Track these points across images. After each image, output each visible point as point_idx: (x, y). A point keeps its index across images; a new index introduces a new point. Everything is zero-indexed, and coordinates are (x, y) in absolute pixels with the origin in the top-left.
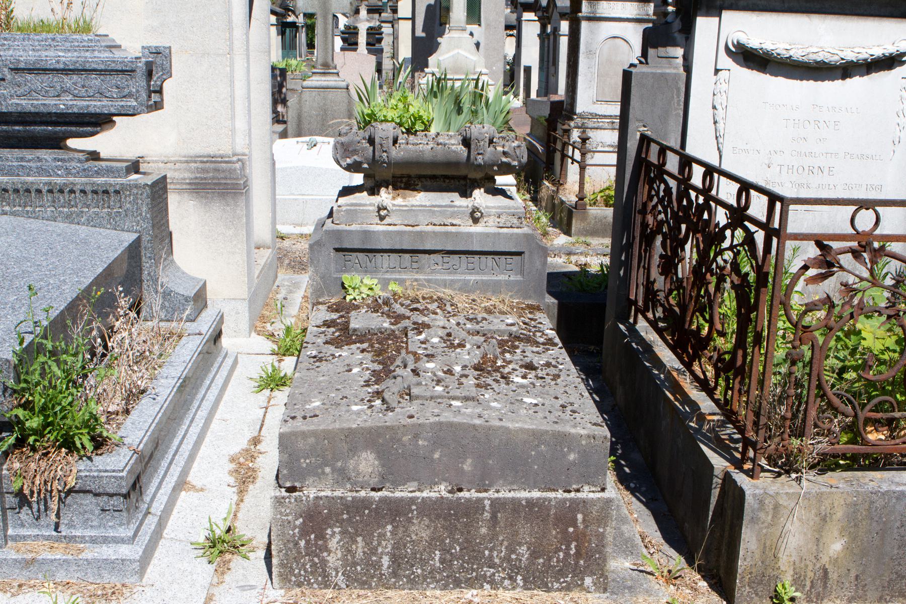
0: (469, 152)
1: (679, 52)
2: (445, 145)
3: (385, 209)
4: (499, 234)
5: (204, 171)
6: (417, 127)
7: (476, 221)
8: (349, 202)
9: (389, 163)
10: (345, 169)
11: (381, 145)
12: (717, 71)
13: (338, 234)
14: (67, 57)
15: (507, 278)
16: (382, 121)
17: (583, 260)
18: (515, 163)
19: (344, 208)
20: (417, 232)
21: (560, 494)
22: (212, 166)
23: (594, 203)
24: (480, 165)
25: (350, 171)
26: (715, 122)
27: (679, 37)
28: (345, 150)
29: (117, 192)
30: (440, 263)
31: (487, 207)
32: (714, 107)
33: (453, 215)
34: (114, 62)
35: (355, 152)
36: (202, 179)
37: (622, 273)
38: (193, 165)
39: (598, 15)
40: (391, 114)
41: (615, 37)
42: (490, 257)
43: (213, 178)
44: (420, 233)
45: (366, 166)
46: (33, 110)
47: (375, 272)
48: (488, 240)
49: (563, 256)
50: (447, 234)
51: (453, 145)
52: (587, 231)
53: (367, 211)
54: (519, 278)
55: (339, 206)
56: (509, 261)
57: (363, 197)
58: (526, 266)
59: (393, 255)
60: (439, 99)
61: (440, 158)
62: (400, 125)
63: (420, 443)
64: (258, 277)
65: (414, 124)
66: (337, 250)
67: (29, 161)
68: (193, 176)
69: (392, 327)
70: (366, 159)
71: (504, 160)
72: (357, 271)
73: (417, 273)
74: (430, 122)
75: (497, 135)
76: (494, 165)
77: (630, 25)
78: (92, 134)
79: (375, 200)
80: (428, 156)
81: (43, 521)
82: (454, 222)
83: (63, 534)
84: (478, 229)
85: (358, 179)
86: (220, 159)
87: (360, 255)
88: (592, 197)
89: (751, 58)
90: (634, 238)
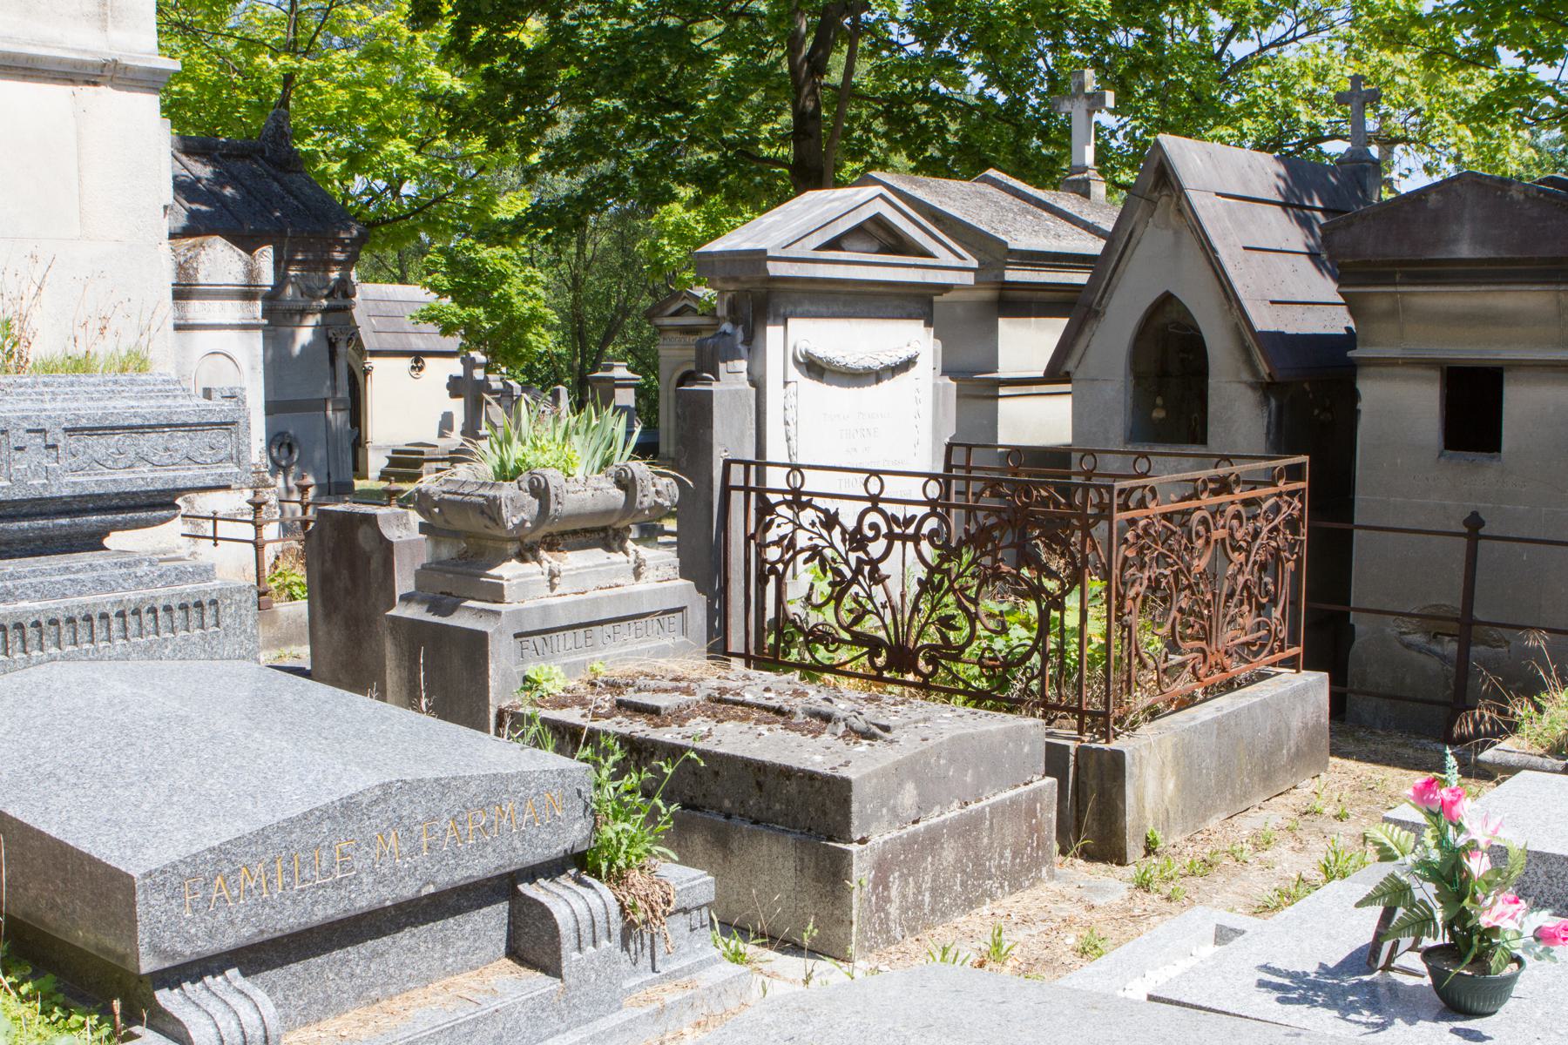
1: (742, 365)
12: (786, 383)
14: (148, 409)
18: (667, 503)
19: (515, 582)
21: (1022, 789)
26: (788, 439)
27: (743, 350)
29: (214, 602)
32: (787, 423)
34: (26, 418)
46: (98, 490)
66: (516, 636)
67: (78, 571)
78: (148, 524)
80: (589, 506)
81: (640, 966)
83: (663, 972)
84: (641, 586)
89: (815, 368)
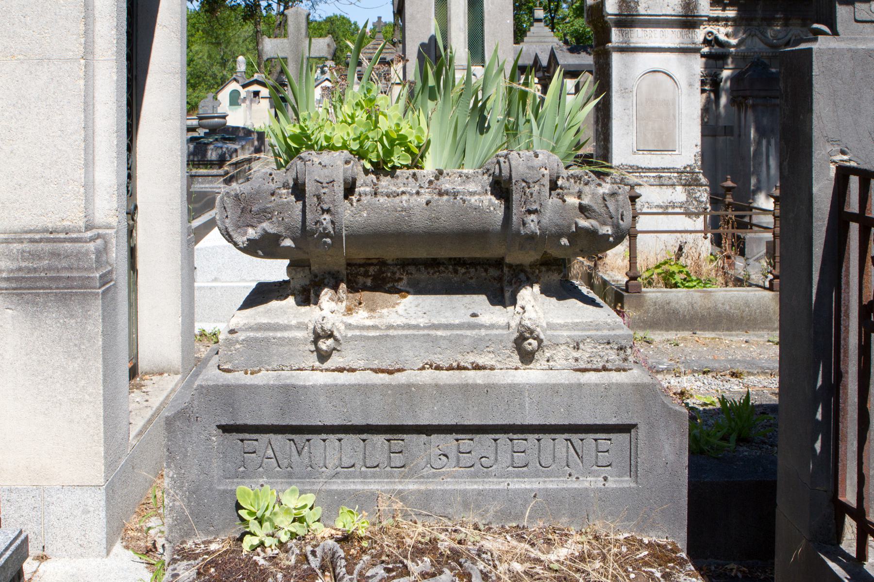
2: (455, 195)
3: (331, 335)
4: (580, 386)
5: (35, 256)
6: (396, 160)
7: (527, 357)
8: (252, 322)
10: (245, 250)
11: (319, 197)
16: (322, 148)
19: (241, 336)
20: (400, 386)
22: (48, 247)
24: (532, 237)
25: (256, 255)
28: (243, 210)
30: (452, 455)
31: (550, 326)
33: (477, 346)
35: (265, 214)
36: (29, 270)
37: (818, 446)
38: (16, 247)
39: (632, 45)
40: (340, 134)
41: (654, 71)
43: (50, 268)
44: (406, 388)
45: (288, 243)
47: (310, 476)
48: (557, 399)
50: (466, 389)
52: (644, 322)
53: (291, 342)
54: (627, 482)
55: (232, 332)
56: (604, 445)
57: (285, 310)
58: (642, 457)
59: (347, 438)
60: (440, 101)
61: (447, 221)
62: (361, 155)
64: (140, 433)
65: (389, 153)
66: (226, 429)
68: (13, 265)
70: (288, 228)
71: (583, 223)
74: (424, 148)
75: (565, 173)
76: (560, 236)
77: (673, 56)
79: (311, 315)
80: (420, 220)
82: (481, 361)
84: (532, 375)
85: (276, 270)
86: (62, 236)
87: (278, 439)
88: (647, 274)
90: (839, 375)
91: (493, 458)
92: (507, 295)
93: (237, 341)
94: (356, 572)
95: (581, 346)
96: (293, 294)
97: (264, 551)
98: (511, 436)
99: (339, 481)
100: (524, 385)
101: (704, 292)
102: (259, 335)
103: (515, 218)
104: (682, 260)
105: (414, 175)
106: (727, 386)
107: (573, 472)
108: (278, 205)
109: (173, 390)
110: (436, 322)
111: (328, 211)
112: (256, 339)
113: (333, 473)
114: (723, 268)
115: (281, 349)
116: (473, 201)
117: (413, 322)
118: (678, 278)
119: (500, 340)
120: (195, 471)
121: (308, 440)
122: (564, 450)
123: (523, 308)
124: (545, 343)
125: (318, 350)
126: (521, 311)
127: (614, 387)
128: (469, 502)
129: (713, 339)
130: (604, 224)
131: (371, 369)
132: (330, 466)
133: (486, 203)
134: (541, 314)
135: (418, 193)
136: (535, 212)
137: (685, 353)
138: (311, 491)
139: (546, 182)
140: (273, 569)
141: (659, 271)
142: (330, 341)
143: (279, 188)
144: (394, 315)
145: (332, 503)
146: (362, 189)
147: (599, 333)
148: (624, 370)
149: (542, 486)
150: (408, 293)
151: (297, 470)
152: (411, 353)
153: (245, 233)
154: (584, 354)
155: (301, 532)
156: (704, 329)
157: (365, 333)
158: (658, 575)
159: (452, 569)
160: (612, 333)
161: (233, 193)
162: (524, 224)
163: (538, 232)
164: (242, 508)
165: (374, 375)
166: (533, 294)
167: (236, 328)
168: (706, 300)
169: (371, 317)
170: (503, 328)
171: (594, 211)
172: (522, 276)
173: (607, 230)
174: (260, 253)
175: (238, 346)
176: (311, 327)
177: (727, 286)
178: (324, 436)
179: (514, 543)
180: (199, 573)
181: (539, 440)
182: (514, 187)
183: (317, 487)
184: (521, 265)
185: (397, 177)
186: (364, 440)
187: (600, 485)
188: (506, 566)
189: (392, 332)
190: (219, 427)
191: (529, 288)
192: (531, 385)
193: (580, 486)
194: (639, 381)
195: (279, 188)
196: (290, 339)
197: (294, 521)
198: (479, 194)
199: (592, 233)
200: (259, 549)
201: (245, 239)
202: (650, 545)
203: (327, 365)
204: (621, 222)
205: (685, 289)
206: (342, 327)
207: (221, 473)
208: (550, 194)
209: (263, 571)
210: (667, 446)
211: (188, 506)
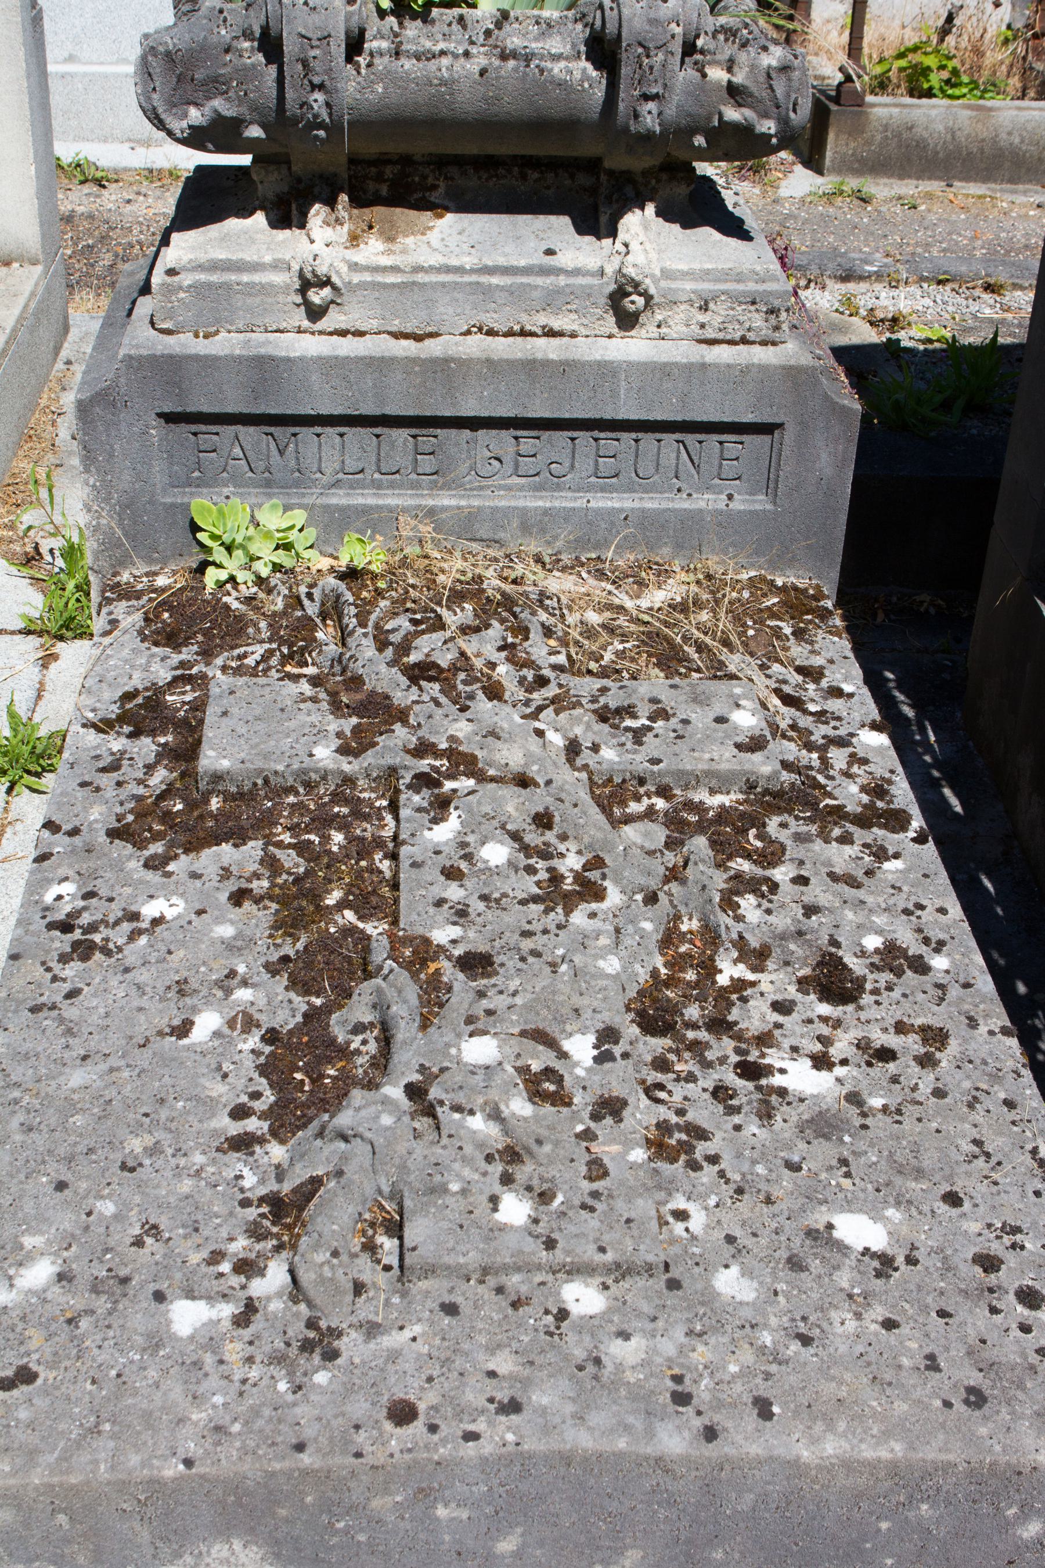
0: (612, 87)
2: (528, 58)
4: (704, 366)
7: (627, 321)
9: (334, 128)
10: (184, 142)
11: (305, 63)
13: (169, 369)
15: (720, 502)
17: (888, 300)
19: (186, 279)
20: (434, 361)
23: (882, 85)
24: (648, 137)
30: (508, 459)
31: (667, 274)
33: (552, 301)
35: (215, 85)
42: (669, 438)
44: (442, 365)
45: (255, 132)
47: (297, 484)
48: (667, 385)
49: (830, 283)
50: (531, 367)
51: (557, 58)
52: (862, 161)
53: (265, 289)
54: (761, 503)
56: (732, 449)
57: (248, 236)
58: (786, 468)
61: (511, 104)
63: (441, 1512)
66: (170, 418)
69: (348, 766)
70: (254, 108)
71: (733, 114)
72: (237, 480)
73: (434, 486)
76: (693, 131)
80: (468, 100)
82: (556, 324)
87: (249, 434)
88: (878, 70)
91: (567, 464)
92: (604, 219)
93: (181, 288)
94: (370, 624)
95: (711, 305)
96: (262, 208)
97: (236, 588)
98: (596, 434)
99: (341, 492)
100: (620, 363)
101: (980, 108)
102: (214, 278)
103: (621, 106)
104: (951, 40)
105: (461, 19)
106: (974, 307)
107: (684, 486)
108: (237, 71)
109: (33, 294)
110: (490, 263)
111: (321, 87)
112: (210, 285)
113: (333, 480)
114: (1024, 58)
115: (249, 301)
116: (556, 71)
117: (454, 262)
118: (935, 80)
119: (587, 293)
120: (127, 476)
121: (295, 435)
122: (674, 455)
123: (626, 245)
124: (656, 300)
125: (307, 304)
126: (623, 249)
127: (754, 370)
128: (530, 524)
129: (980, 197)
130: (765, 115)
131: (389, 333)
132: (329, 471)
133: (577, 75)
134: (653, 255)
135: (467, 54)
136: (655, 97)
137: (926, 223)
138: (300, 506)
139: (677, 47)
140: (252, 615)
141: (903, 63)
142: (326, 291)
143: (237, 38)
144: (424, 248)
145: (334, 525)
146: (375, 44)
147: (741, 287)
148: (774, 344)
149: (637, 505)
150: (448, 209)
151: (278, 476)
152: (451, 311)
153: (185, 115)
154: (714, 318)
155: (288, 562)
156: (967, 179)
157: (379, 278)
158: (788, 631)
159: (502, 621)
160: (761, 287)
161: (161, 49)
162: (636, 116)
163: (658, 129)
164: (202, 530)
165: (392, 342)
166: (646, 227)
167: (177, 267)
168: (980, 126)
169: (389, 252)
170: (592, 275)
171: (751, 95)
172: (629, 190)
173: (768, 126)
174: (210, 146)
175: (182, 295)
176: (296, 267)
177: (1023, 97)
178: (318, 430)
179: (592, 581)
180: (147, 619)
181: (636, 441)
182: (624, 56)
183: (309, 501)
184: (628, 172)
185: (433, 22)
186: (378, 436)
187: (722, 506)
188: (577, 616)
189: (420, 278)
190: (160, 415)
191: (637, 211)
192: (629, 363)
193: (694, 506)
194: (792, 362)
195: (237, 38)
196: (263, 286)
197: (277, 548)
198: (567, 59)
199: (745, 131)
200: (229, 586)
201: (184, 124)
202: (784, 589)
203: (320, 325)
204: (792, 115)
205: (945, 102)
206: (344, 269)
207: (166, 480)
208: (682, 63)
209: (239, 618)
210: (824, 456)
211: (120, 524)
